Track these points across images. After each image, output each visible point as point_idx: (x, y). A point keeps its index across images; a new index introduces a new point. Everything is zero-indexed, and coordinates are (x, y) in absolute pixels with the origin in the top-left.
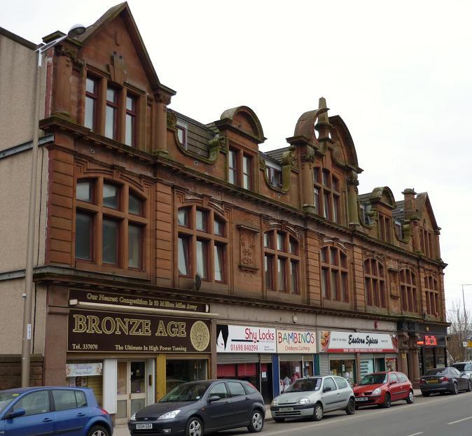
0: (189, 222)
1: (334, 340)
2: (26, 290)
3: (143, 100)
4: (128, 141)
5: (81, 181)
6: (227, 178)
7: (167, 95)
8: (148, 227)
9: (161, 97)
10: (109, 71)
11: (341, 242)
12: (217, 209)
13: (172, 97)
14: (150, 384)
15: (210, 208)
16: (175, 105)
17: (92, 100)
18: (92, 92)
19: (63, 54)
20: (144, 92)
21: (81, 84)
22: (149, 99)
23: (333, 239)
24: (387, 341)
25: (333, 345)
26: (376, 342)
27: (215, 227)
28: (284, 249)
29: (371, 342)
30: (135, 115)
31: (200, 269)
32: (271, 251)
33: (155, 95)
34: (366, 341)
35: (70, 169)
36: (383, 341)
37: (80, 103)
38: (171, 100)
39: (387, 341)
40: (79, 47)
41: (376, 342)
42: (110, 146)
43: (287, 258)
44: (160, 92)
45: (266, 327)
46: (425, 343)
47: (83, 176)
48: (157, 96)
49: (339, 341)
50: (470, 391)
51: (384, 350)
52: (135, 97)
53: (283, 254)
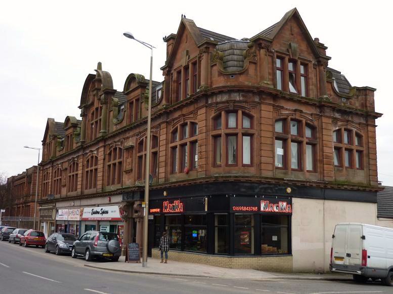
0: (286, 129)
1: (85, 213)
2: (274, 195)
3: (311, 66)
4: (303, 95)
5: (277, 121)
6: (275, 85)
7: (325, 60)
8: (365, 152)
9: (322, 63)
10: (289, 52)
11: (306, 113)
12: (307, 119)
13: (329, 61)
14: (85, 265)
15: (301, 119)
16: (331, 65)
17: (280, 72)
18: (280, 67)
19: (263, 48)
20: (310, 61)
21: (274, 63)
22: (314, 65)
23: (292, 110)
24: (115, 211)
25: (84, 216)
26: (107, 212)
27: (356, 140)
28: (350, 141)
29: (103, 213)
30: (306, 76)
31: (293, 163)
32: (340, 145)
33: (317, 61)
34: (101, 212)
35: (270, 115)
36: (112, 212)
37: (274, 75)
38: (329, 63)
39: (115, 211)
40: (271, 42)
41: (107, 212)
42: (304, 100)
43: (341, 148)
44: (321, 59)
45: (68, 202)
46: (161, 210)
47: (278, 117)
48: (319, 62)
49: (87, 213)
50: (388, 285)
51: (112, 219)
52: (306, 66)
53: (349, 147)
